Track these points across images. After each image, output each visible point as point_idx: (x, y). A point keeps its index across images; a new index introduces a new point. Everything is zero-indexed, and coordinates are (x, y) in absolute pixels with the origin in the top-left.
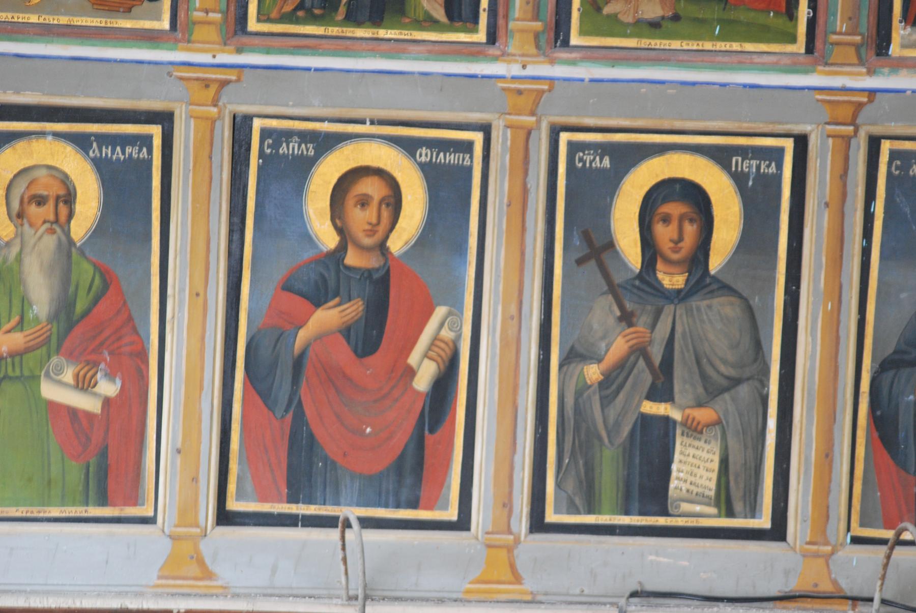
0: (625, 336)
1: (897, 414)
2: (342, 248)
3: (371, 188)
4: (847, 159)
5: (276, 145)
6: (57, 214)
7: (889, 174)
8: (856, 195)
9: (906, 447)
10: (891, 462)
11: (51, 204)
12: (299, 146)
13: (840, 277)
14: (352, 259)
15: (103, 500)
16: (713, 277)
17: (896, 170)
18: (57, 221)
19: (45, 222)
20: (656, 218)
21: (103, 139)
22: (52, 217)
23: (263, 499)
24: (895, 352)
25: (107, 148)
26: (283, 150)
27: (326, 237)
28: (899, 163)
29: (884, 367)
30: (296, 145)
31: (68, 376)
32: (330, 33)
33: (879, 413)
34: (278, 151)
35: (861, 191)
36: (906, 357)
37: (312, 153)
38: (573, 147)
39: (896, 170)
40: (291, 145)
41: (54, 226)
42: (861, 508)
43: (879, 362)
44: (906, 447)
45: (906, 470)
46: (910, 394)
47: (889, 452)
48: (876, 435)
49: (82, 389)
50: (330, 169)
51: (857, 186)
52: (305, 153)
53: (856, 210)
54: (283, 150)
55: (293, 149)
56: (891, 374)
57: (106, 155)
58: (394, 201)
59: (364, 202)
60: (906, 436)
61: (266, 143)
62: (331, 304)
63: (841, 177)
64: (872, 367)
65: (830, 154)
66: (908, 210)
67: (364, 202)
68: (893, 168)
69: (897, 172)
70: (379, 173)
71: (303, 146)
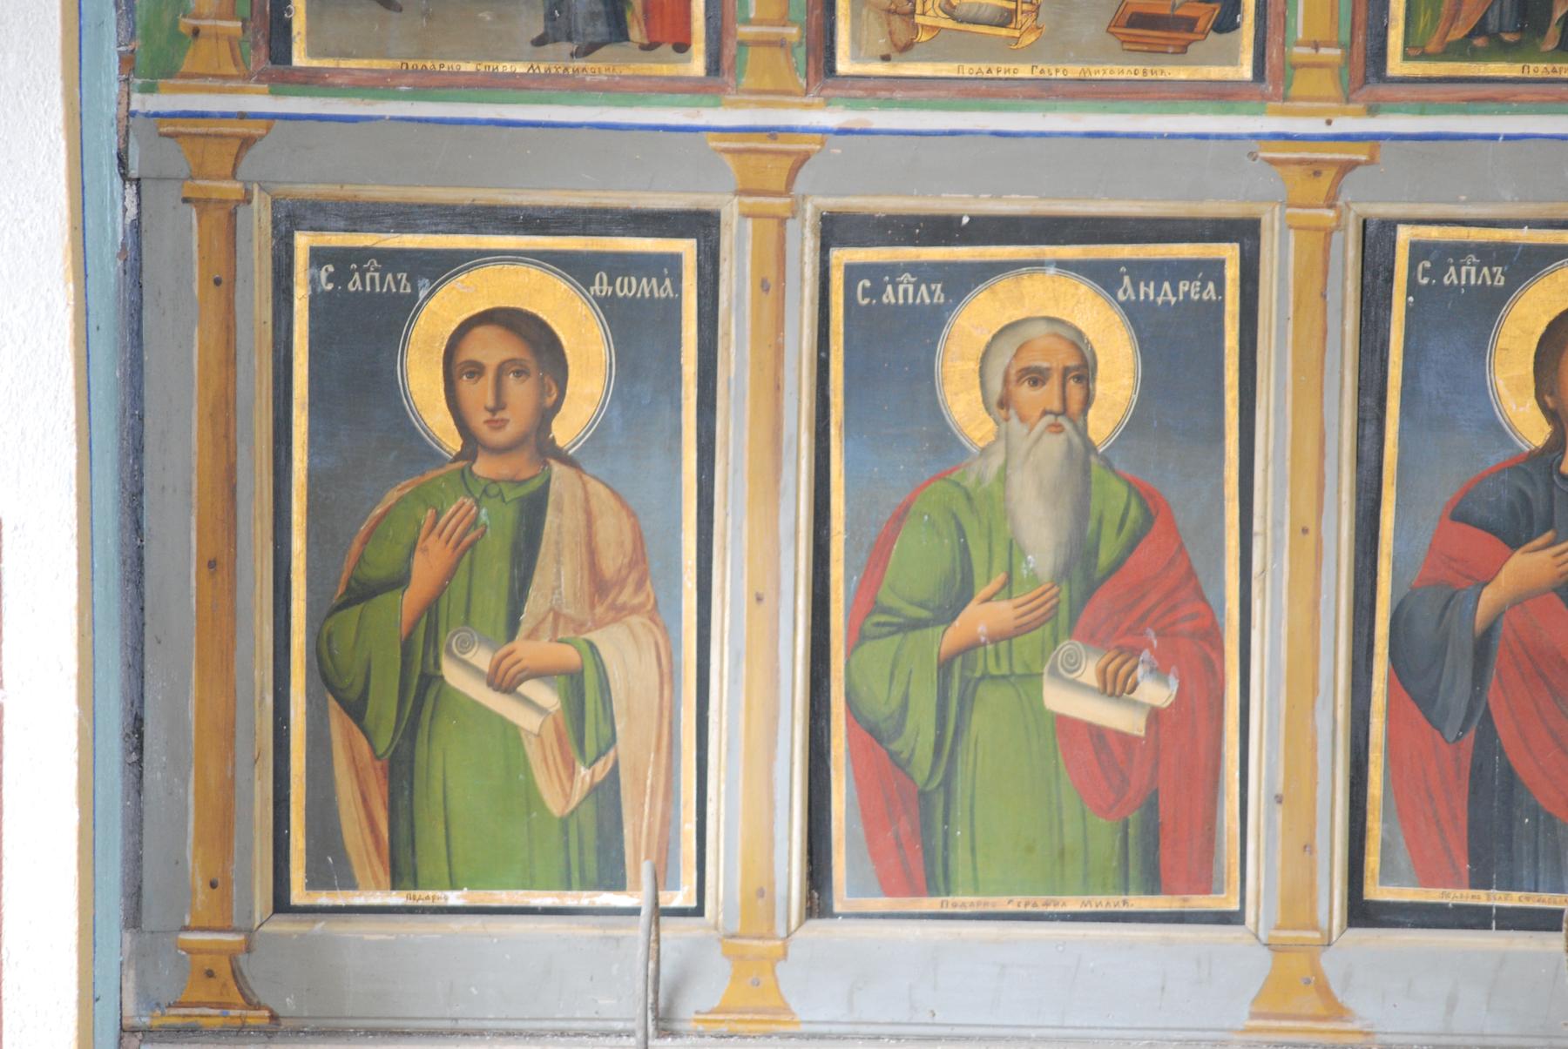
5: (875, 292)
6: (1064, 400)
11: (490, 375)
12: (1478, 272)
15: (1153, 884)
18: (1064, 411)
19: (1045, 413)
21: (1142, 270)
22: (1056, 405)
23: (1427, 882)
25: (1147, 285)
26: (888, 297)
28: (868, 284)
30: (1473, 270)
31: (1089, 673)
32: (1532, 74)
37: (1500, 281)
38: (342, 261)
40: (901, 288)
41: (1061, 420)
49: (1112, 695)
52: (927, 301)
54: (888, 297)
55: (906, 291)
57: (1146, 295)
62: (1539, 542)
69: (866, 301)
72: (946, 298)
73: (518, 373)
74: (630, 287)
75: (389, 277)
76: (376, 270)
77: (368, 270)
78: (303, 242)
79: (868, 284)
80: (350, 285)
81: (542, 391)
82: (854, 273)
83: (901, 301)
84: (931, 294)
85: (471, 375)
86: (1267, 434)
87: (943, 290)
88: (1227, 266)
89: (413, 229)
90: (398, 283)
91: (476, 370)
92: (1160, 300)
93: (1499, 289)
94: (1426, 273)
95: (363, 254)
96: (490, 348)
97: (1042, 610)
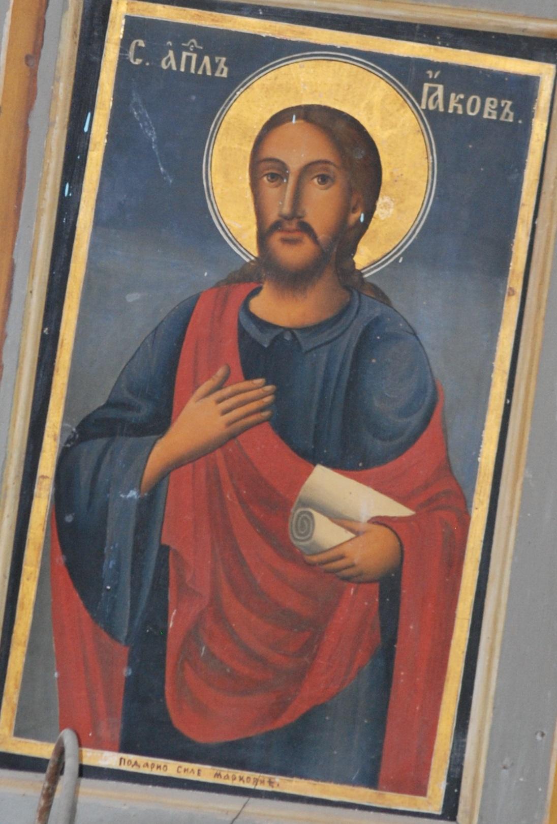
1: (104, 523)
4: (40, 26)
5: (153, 54)
7: (123, 62)
8: (53, 96)
9: (115, 588)
10: (85, 615)
12: (199, 61)
13: (12, 253)
15: (371, 780)
21: (459, 79)
24: (109, 404)
26: (168, 62)
28: (142, 43)
29: (86, 430)
30: (194, 56)
33: (69, 519)
35: (63, 90)
36: (130, 415)
42: (21, 699)
43: (77, 420)
44: (115, 588)
45: (112, 632)
46: (132, 488)
47: (83, 596)
48: (60, 560)
50: (252, 106)
51: (56, 79)
52: (209, 73)
53: (51, 124)
54: (168, 62)
55: (189, 59)
56: (101, 443)
60: (118, 568)
61: (133, 46)
63: (27, 58)
64: (63, 429)
65: (9, 14)
66: (152, 135)
68: (131, 54)
69: (138, 62)
71: (207, 59)
72: (516, 118)
73: (324, 179)
75: (207, 59)
76: (195, 50)
77: (187, 49)
79: (142, 43)
81: (346, 210)
83: (182, 69)
84: (214, 66)
85: (274, 177)
86: (542, 282)
87: (511, 108)
91: (279, 173)
93: (510, 123)
94: (139, 52)
95: (181, 33)
96: (300, 148)
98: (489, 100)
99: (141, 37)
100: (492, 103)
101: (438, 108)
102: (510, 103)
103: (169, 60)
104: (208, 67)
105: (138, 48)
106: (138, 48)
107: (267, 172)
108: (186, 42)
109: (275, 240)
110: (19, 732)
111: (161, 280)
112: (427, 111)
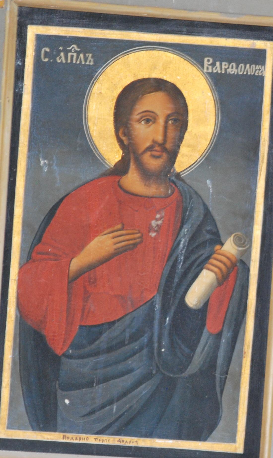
0: (114, 238)
2: (121, 169)
3: (155, 103)
5: (52, 55)
14: (133, 181)
16: (178, 175)
17: (45, 57)
20: (136, 116)
26: (61, 59)
27: (112, 154)
28: (48, 50)
30: (75, 55)
34: (55, 59)
37: (90, 62)
39: (45, 57)
40: (70, 54)
52: (83, 63)
54: (61, 59)
55: (72, 56)
58: (179, 117)
59: (150, 118)
67: (150, 118)
68: (42, 56)
69: (46, 60)
70: (160, 85)
71: (81, 56)
74: (221, 67)
75: (81, 56)
76: (76, 51)
77: (70, 51)
78: (33, 31)
79: (48, 50)
80: (58, 58)
82: (41, 40)
83: (69, 61)
84: (86, 59)
87: (92, 57)
88: (40, 33)
89: (199, 34)
90: (86, 59)
92: (78, 62)
95: (66, 41)
97: (193, 169)
98: (224, 63)
99: (46, 46)
100: (225, 65)
101: (62, 61)
102: (90, 55)
103: (216, 68)
104: (83, 60)
105: (45, 52)
106: (46, 52)
107: (171, 118)
108: (69, 47)
109: (149, 153)
110: (11, 426)
111: (65, 176)
112: (209, 73)
